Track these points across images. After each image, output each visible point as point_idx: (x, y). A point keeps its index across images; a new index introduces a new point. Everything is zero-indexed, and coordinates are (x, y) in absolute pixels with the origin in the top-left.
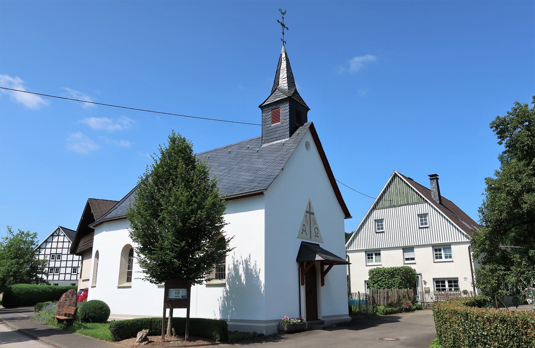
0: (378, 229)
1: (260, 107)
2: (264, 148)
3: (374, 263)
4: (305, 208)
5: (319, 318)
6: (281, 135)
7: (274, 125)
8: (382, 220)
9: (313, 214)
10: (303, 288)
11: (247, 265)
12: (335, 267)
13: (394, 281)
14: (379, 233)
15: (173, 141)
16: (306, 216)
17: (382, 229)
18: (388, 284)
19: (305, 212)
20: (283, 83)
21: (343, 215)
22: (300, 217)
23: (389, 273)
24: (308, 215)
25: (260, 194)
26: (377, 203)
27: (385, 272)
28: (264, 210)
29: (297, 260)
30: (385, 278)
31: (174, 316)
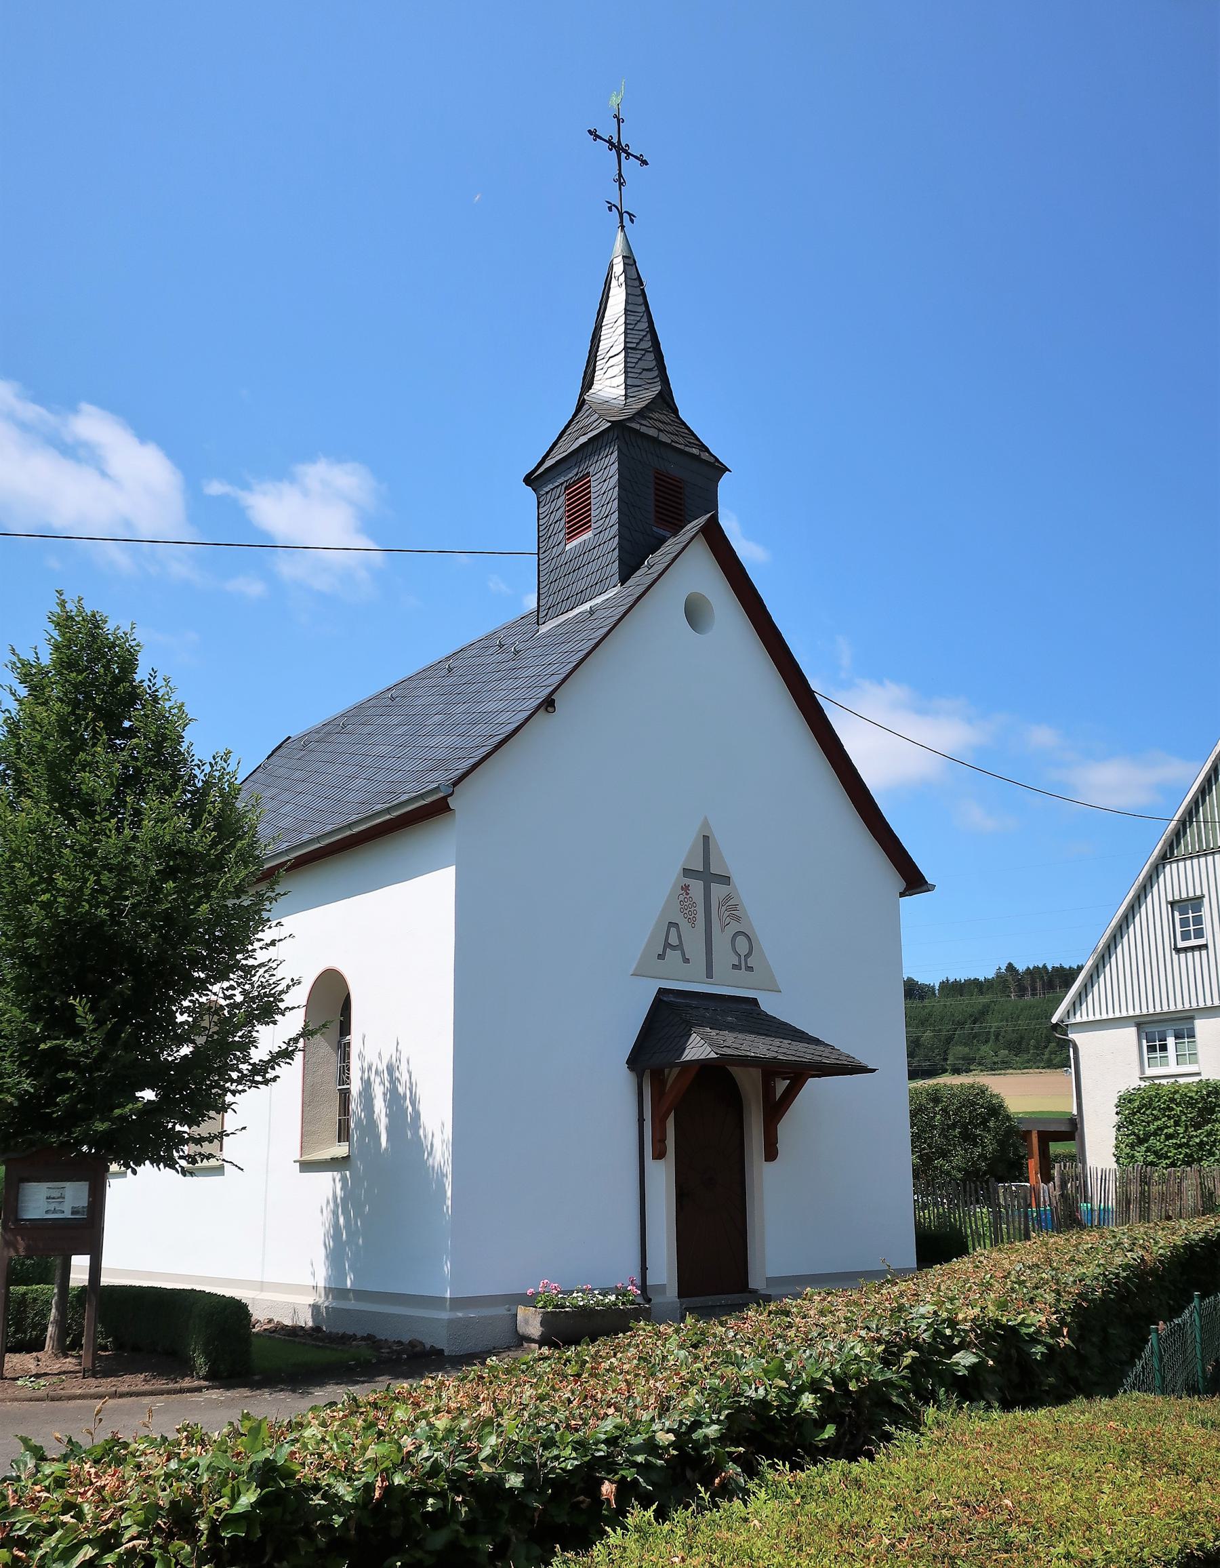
0: (1186, 936)
1: (528, 480)
2: (547, 635)
3: (1173, 1068)
4: (680, 851)
5: (752, 1286)
6: (593, 579)
7: (575, 543)
8: (1195, 902)
9: (725, 880)
10: (662, 1176)
11: (394, 1081)
12: (813, 1085)
13: (1209, 1134)
14: (1186, 950)
15: (64, 622)
16: (686, 888)
17: (1199, 934)
18: (1187, 1145)
19: (678, 870)
20: (610, 384)
21: (896, 882)
22: (654, 891)
23: (1191, 1103)
24: (697, 887)
25: (433, 809)
26: (1179, 834)
27: (1172, 1100)
28: (452, 870)
29: (635, 1061)
30: (1177, 1124)
31: (105, 1280)
